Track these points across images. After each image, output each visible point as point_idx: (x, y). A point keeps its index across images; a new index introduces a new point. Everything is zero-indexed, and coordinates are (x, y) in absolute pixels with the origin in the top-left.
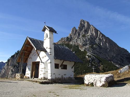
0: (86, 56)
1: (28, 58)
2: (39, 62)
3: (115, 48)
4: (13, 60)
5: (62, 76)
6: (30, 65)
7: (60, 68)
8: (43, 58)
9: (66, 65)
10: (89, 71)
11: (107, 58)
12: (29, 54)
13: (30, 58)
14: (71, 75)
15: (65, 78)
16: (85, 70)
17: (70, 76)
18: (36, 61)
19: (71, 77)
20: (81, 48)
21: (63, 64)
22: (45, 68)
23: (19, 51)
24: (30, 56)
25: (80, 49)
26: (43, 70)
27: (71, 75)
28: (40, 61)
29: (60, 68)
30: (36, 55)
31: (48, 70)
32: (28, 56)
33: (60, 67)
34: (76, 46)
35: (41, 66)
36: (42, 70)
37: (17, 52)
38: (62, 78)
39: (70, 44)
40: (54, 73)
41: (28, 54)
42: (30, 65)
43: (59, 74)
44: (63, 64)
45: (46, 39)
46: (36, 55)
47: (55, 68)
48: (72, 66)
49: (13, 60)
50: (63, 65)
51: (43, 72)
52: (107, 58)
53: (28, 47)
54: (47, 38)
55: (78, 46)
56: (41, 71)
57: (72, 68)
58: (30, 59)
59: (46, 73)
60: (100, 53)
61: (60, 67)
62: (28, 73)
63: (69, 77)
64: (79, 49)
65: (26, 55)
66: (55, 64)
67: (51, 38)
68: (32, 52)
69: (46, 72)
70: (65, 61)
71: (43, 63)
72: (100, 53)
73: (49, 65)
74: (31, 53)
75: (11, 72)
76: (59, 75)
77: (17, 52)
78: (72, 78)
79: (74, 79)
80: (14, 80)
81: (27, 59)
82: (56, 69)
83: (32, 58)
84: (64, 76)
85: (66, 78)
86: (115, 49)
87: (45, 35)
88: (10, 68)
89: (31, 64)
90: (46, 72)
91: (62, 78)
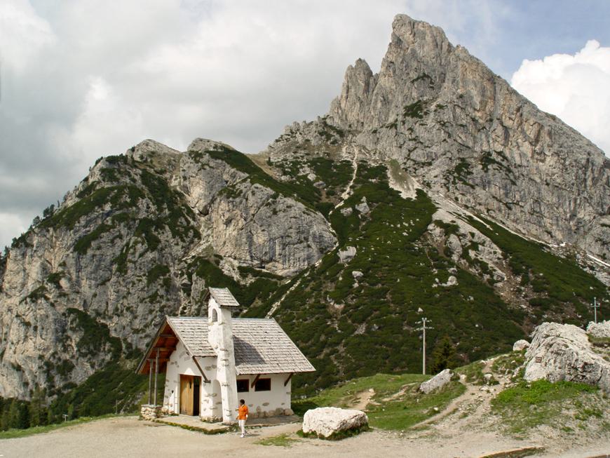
0: (431, 227)
5: (258, 408)
7: (252, 390)
11: (549, 233)
13: (172, 363)
14: (283, 404)
15: (267, 411)
16: (421, 304)
19: (282, 409)
20: (401, 180)
23: (55, 208)
25: (396, 188)
29: (252, 390)
33: (252, 387)
34: (373, 169)
37: (42, 217)
38: (259, 413)
39: (335, 159)
41: (166, 353)
48: (286, 379)
52: (549, 233)
55: (380, 171)
57: (285, 385)
59: (218, 406)
60: (510, 209)
61: (252, 387)
62: (172, 401)
63: (278, 410)
64: (387, 184)
66: (238, 381)
71: (209, 382)
72: (506, 204)
74: (176, 350)
77: (42, 217)
78: (284, 410)
79: (292, 412)
80: (149, 426)
84: (263, 409)
85: (270, 412)
91: (259, 413)
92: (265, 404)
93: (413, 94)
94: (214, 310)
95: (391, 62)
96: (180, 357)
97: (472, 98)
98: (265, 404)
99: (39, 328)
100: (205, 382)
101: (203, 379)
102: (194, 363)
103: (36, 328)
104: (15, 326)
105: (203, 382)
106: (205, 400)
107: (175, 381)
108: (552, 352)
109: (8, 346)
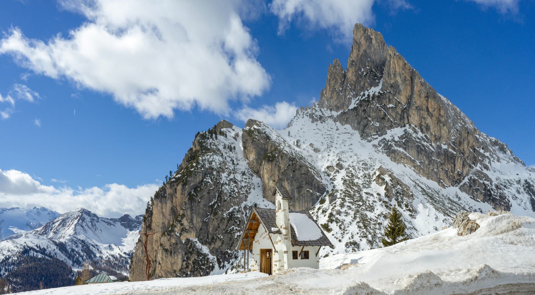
3: (466, 142)
4: (162, 208)
7: (299, 258)
21: (303, 250)
22: (280, 261)
26: (278, 263)
30: (266, 238)
32: (253, 238)
33: (299, 256)
35: (275, 257)
36: (276, 263)
41: (252, 235)
44: (303, 250)
46: (265, 237)
49: (162, 208)
50: (303, 251)
51: (278, 267)
54: (280, 211)
58: (257, 243)
59: (281, 268)
61: (299, 256)
68: (258, 230)
70: (305, 246)
71: (277, 252)
86: (469, 142)
89: (259, 252)
92: (324, 249)
93: (366, 85)
94: (279, 201)
95: (353, 61)
96: (260, 237)
97: (398, 86)
98: (324, 249)
99: (173, 252)
100: (275, 252)
101: (273, 250)
102: (270, 240)
103: (171, 252)
104: (160, 252)
105: (273, 252)
106: (275, 265)
107: (258, 254)
108: (468, 229)
109: (157, 265)
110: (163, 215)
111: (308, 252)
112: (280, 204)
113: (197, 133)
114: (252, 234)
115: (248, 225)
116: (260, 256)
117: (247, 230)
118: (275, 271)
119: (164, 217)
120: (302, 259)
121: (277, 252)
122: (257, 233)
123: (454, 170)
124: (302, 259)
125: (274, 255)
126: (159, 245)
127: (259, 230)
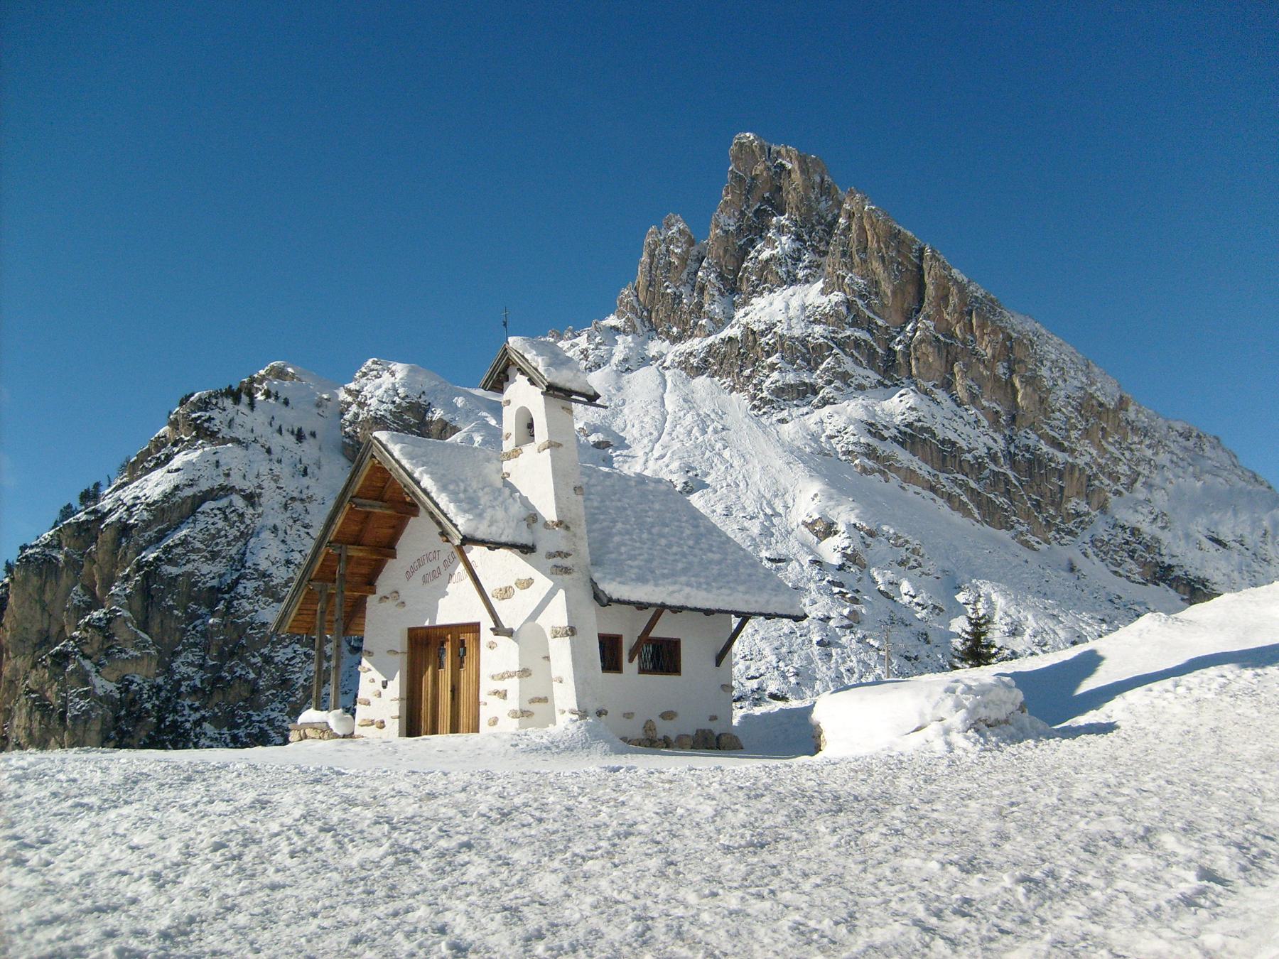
1: (372, 601)
2: (475, 628)
4: (41, 590)
6: (395, 653)
7: (630, 668)
8: (506, 593)
9: (676, 643)
10: (987, 577)
12: (377, 569)
17: (707, 725)
18: (441, 620)
19: (710, 731)
21: (653, 634)
22: (524, 673)
24: (385, 583)
27: (713, 718)
28: (487, 624)
29: (630, 668)
31: (556, 685)
32: (369, 582)
33: (631, 660)
40: (597, 706)
41: (365, 570)
42: (395, 653)
43: (627, 710)
44: (653, 634)
45: (516, 453)
47: (411, 631)
49: (41, 590)
51: (513, 703)
53: (368, 514)
54: (529, 449)
56: (496, 697)
58: (390, 604)
59: (535, 707)
61: (631, 660)
65: (357, 579)
67: (560, 445)
69: (532, 701)
71: (510, 633)
73: (561, 654)
75: (30, 714)
76: (628, 715)
81: (356, 610)
82: (606, 674)
83: (403, 596)
87: (510, 423)
88: (15, 670)
90: (532, 701)
96: (409, 575)
105: (486, 635)
110: (43, 609)
111: (676, 643)
112: (531, 426)
113: (542, 696)
114: (360, 562)
115: (340, 520)
116: (405, 658)
117: (336, 541)
118: (494, 722)
119: (46, 616)
120: (642, 671)
121: (510, 633)
122: (390, 562)
123: (1061, 498)
124: (642, 671)
125: (492, 646)
126: (1063, 903)
127: (403, 545)
